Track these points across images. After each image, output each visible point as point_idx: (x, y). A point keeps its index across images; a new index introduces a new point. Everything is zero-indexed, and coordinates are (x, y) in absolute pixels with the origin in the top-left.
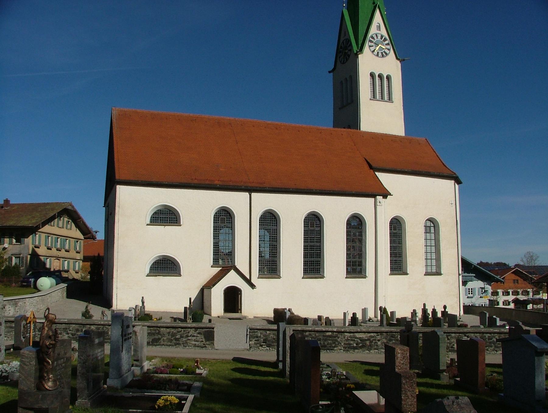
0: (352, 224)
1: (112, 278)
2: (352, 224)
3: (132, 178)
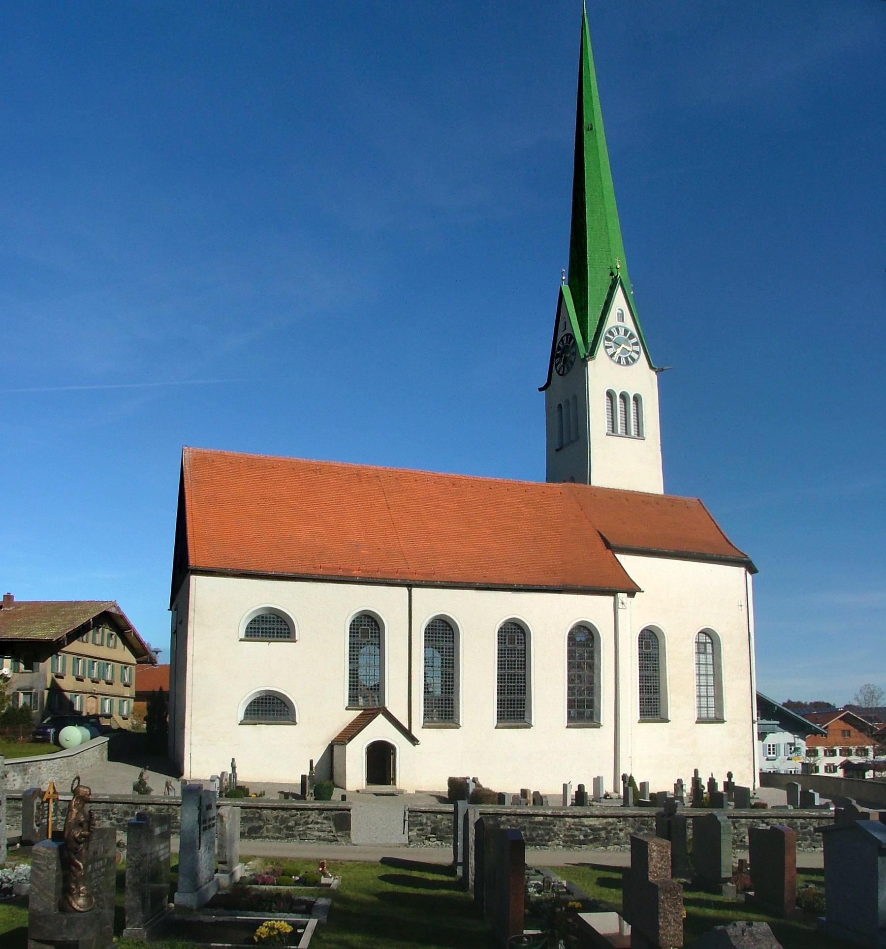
0: (578, 639)
2: (578, 639)
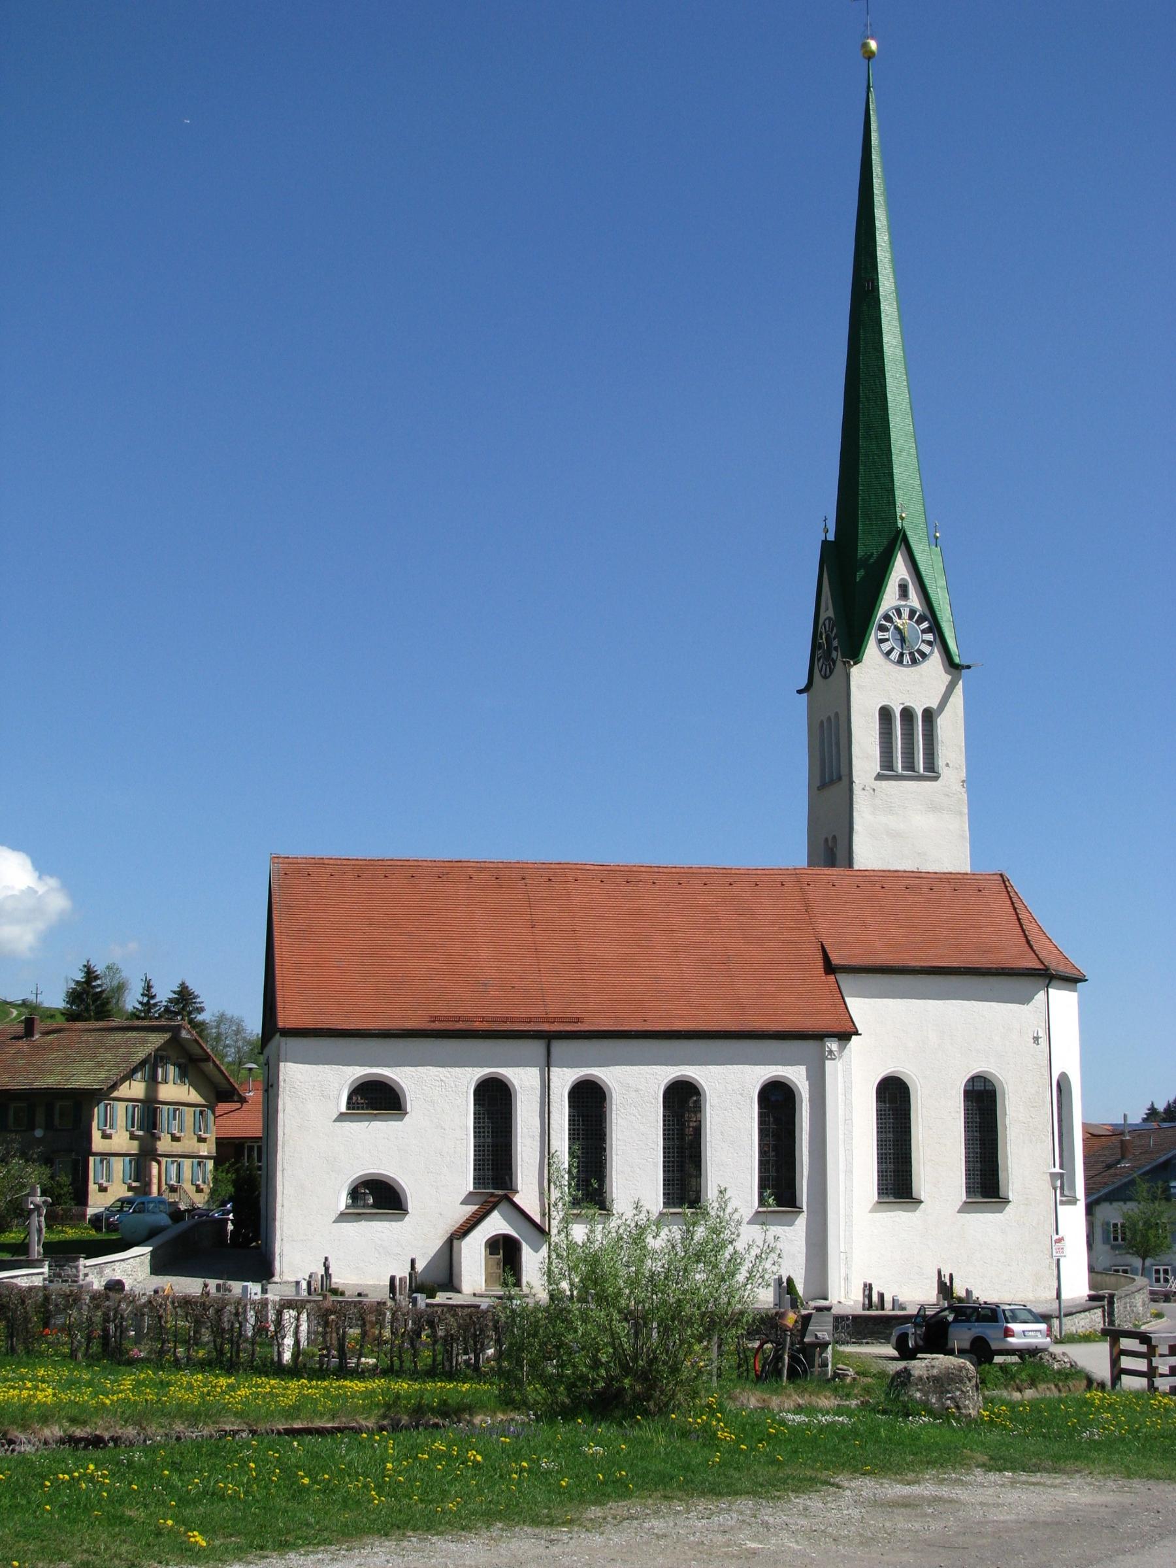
0: (773, 1098)
1: (274, 1219)
2: (773, 1098)
3: (310, 1024)
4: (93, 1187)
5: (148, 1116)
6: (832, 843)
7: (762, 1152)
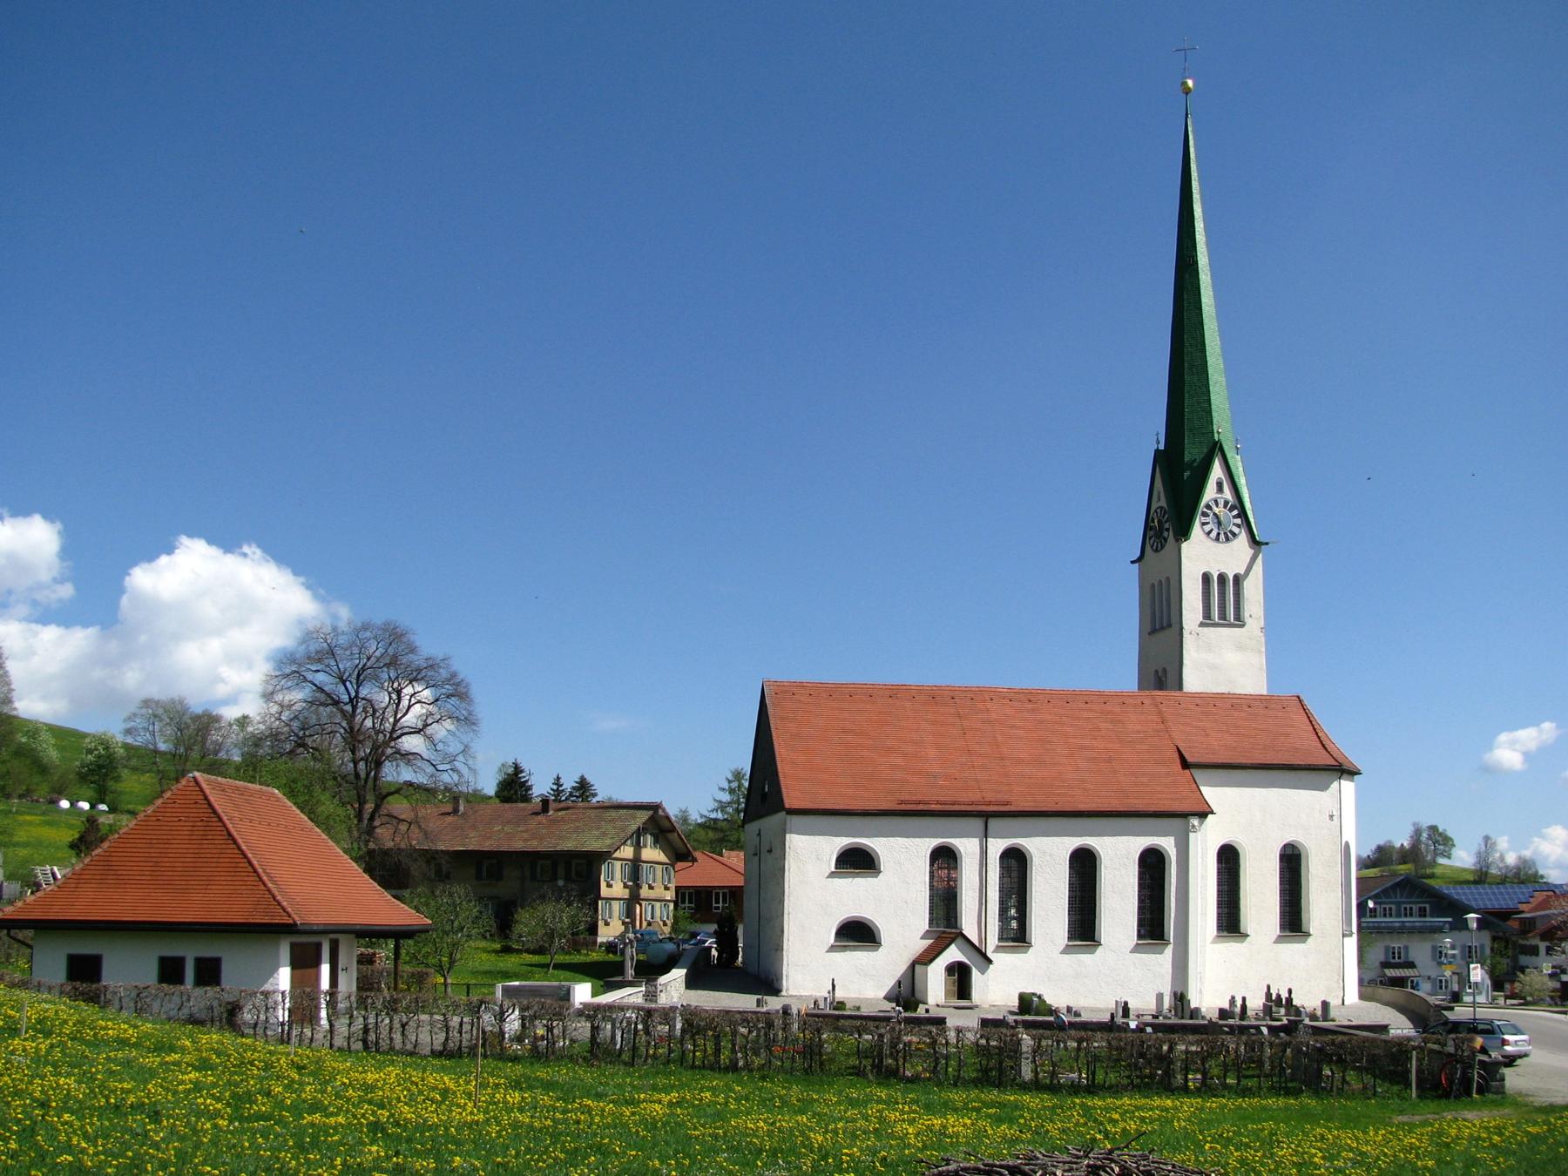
4: (601, 923)
5: (635, 869)
6: (1161, 670)
7: (1141, 901)
